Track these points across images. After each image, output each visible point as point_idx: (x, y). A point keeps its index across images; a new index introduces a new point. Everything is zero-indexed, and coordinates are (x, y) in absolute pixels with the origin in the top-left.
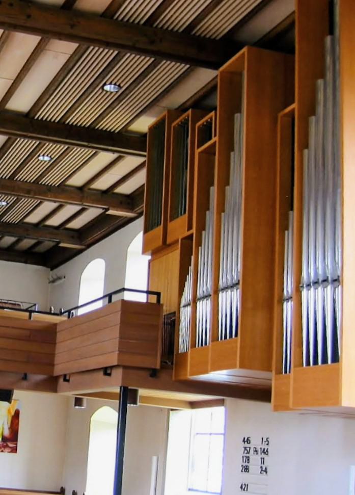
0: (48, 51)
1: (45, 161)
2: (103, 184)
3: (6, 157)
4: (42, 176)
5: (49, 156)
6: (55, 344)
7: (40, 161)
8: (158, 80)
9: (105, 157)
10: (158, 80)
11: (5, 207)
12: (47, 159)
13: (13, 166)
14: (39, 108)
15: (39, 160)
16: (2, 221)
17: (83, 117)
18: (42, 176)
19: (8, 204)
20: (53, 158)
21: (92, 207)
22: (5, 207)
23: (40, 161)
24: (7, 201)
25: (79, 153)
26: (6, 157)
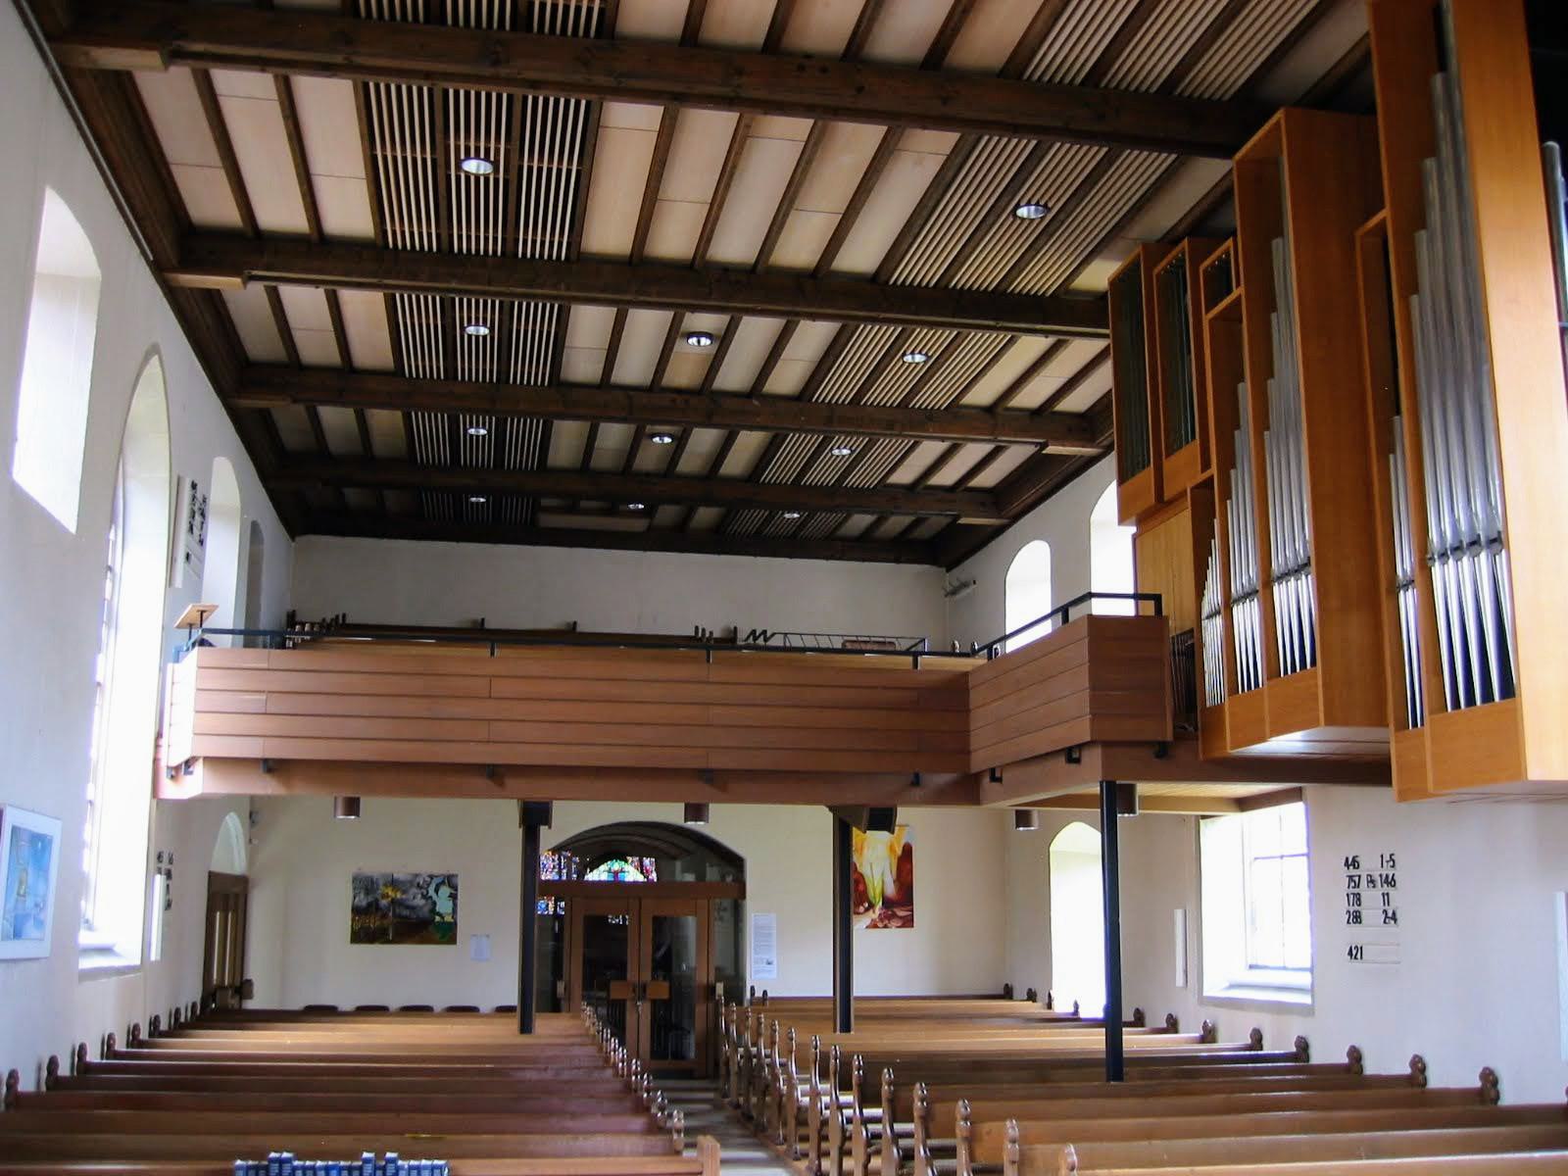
1: (844, 456)
3: (774, 466)
4: (914, 392)
5: (924, 352)
9: (1031, 346)
25: (980, 341)
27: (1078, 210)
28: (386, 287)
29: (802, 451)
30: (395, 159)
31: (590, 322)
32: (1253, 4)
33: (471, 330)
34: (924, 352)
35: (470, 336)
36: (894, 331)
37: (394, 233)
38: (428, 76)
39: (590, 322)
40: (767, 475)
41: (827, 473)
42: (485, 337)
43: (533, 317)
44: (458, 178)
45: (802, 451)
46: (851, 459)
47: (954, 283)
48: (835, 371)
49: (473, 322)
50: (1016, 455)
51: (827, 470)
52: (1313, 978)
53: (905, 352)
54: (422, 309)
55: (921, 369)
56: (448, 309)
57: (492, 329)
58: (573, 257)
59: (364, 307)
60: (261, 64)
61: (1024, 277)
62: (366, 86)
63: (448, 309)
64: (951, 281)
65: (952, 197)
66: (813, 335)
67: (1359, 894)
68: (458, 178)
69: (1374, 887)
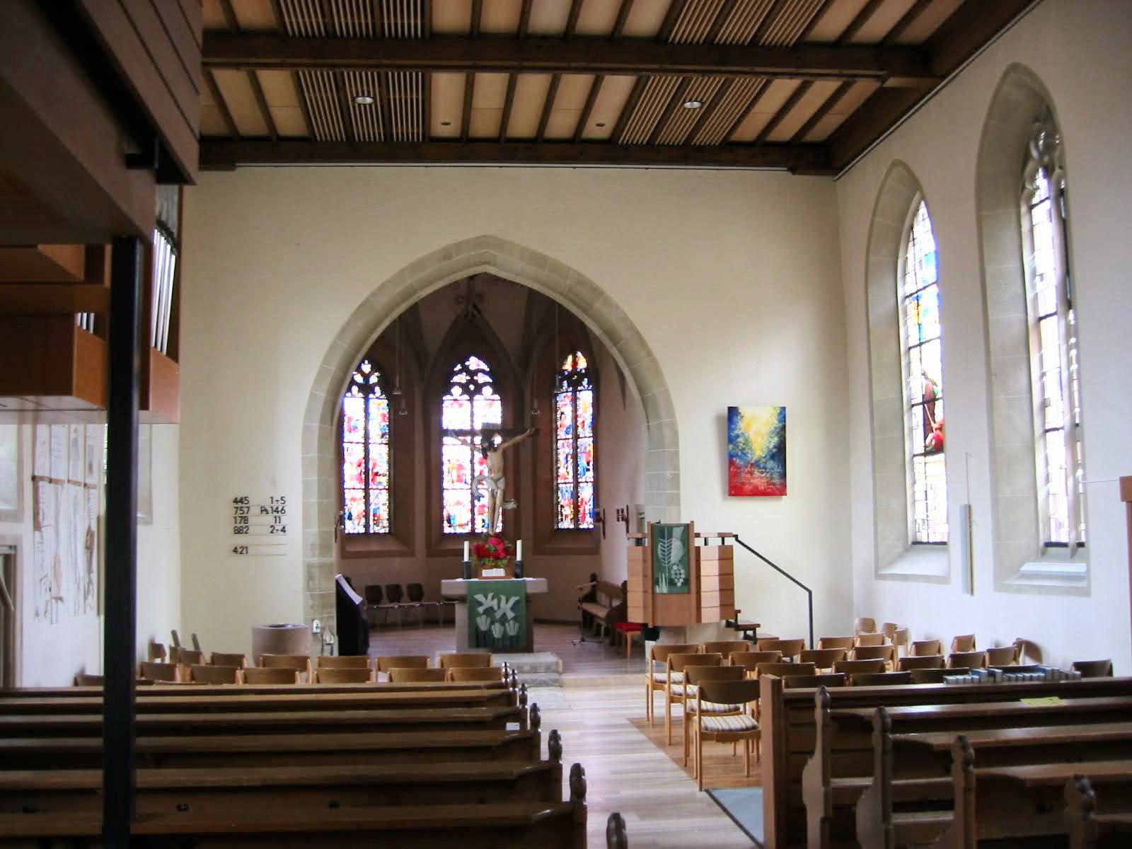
0: (498, 107)
1: (695, 109)
2: (786, 130)
3: (650, 88)
4: (696, 129)
5: (699, 99)
6: (720, 575)
7: (686, 111)
8: (801, 9)
9: (782, 88)
10: (801, 9)
11: (699, 112)
12: (696, 104)
13: (658, 109)
14: (679, 10)
15: (685, 109)
16: (693, 144)
17: (737, 29)
18: (696, 129)
19: (703, 104)
20: (706, 102)
21: (820, 75)
22: (699, 112)
23: (686, 111)
24: (702, 99)
25: (743, 85)
26: (650, 88)
27: (783, 11)
28: (293, 65)
29: (653, 114)
30: (316, 98)
31: (447, 86)
32: (789, 3)
33: (360, 100)
34: (699, 99)
35: (359, 105)
36: (677, 80)
37: (291, 23)
38: (333, 66)
39: (447, 86)
40: (626, 135)
41: (699, 91)
42: (370, 105)
43: (402, 85)
44: (354, 107)
45: (653, 114)
46: (702, 112)
47: (717, 39)
48: (685, 15)
49: (360, 94)
50: (863, 88)
51: (698, 88)
52: (949, 528)
53: (685, 99)
54: (320, 80)
55: (698, 114)
56: (340, 88)
57: (374, 98)
58: (427, 33)
59: (276, 83)
60: (237, 66)
61: (772, 31)
62: (298, 73)
63: (340, 88)
64: (716, 36)
65: (680, 26)
66: (617, 87)
67: (777, 489)
68: (354, 107)
69: (267, 513)
